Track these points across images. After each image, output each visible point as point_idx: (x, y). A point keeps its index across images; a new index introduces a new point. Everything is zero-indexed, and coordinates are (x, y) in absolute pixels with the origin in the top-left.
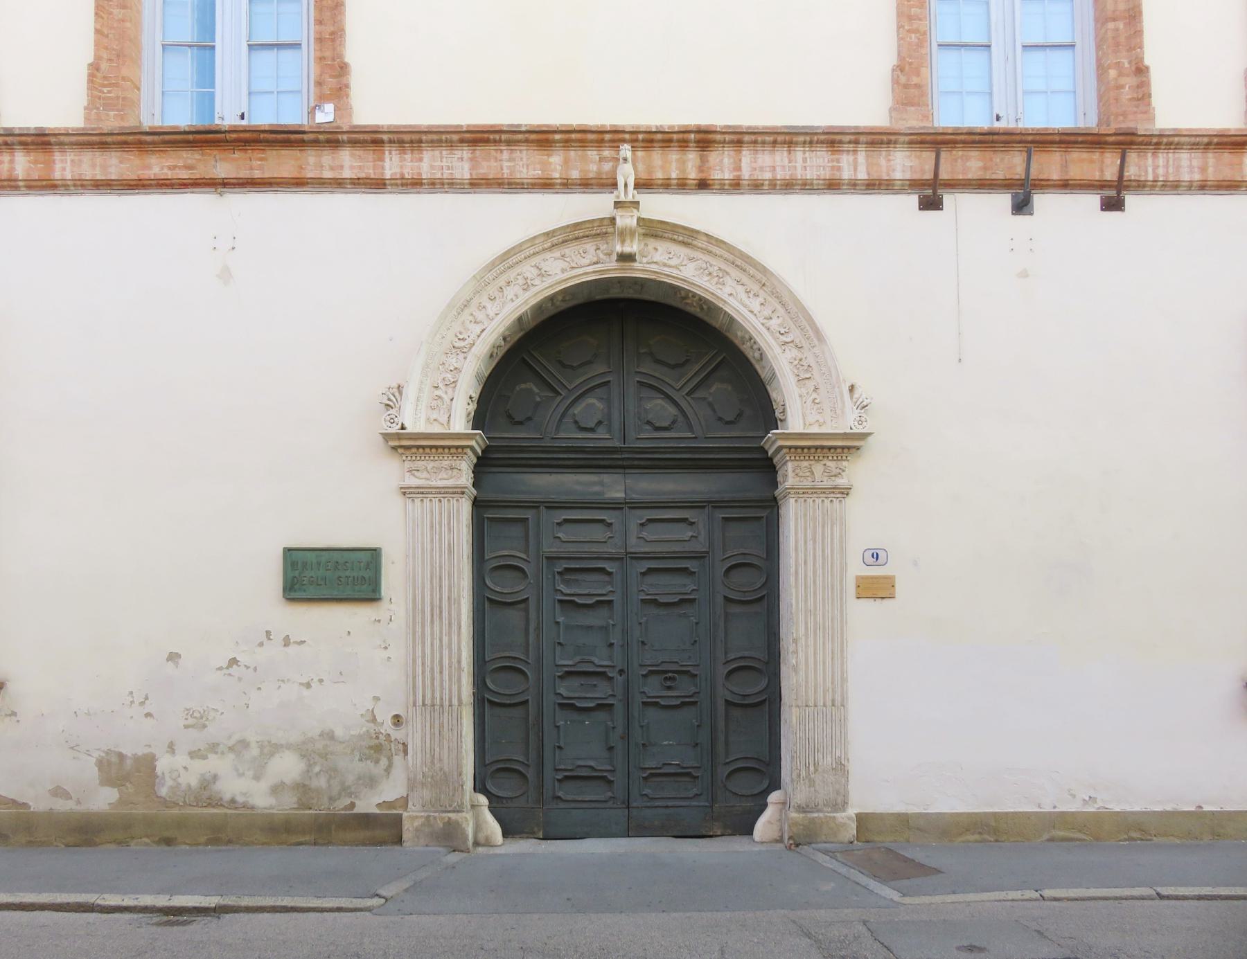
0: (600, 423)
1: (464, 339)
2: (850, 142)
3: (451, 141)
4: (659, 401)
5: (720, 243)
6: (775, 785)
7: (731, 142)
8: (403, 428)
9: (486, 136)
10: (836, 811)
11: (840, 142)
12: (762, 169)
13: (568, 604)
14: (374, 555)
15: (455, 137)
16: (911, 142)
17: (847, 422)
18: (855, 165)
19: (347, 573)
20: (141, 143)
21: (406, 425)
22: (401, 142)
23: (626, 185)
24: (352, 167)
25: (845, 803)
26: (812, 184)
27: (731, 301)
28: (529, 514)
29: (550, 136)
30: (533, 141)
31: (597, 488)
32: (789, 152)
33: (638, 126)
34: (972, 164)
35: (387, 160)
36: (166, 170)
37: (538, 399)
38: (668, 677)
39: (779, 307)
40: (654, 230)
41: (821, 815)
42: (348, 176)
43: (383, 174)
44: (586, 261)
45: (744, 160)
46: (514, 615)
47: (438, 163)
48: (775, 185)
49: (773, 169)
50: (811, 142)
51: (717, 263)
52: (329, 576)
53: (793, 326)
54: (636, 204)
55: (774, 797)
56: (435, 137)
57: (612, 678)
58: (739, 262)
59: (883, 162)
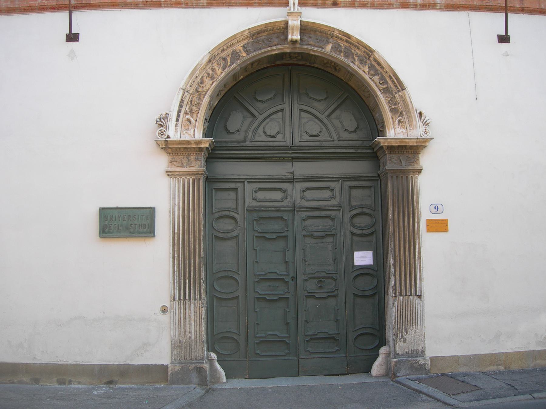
0: (278, 133)
6: (383, 342)
8: (168, 137)
13: (262, 238)
14: (152, 210)
19: (136, 222)
21: (170, 136)
23: (294, 4)
28: (239, 185)
38: (320, 281)
46: (231, 244)
48: (374, 4)
52: (123, 224)
54: (300, 14)
55: (383, 350)
57: (287, 282)
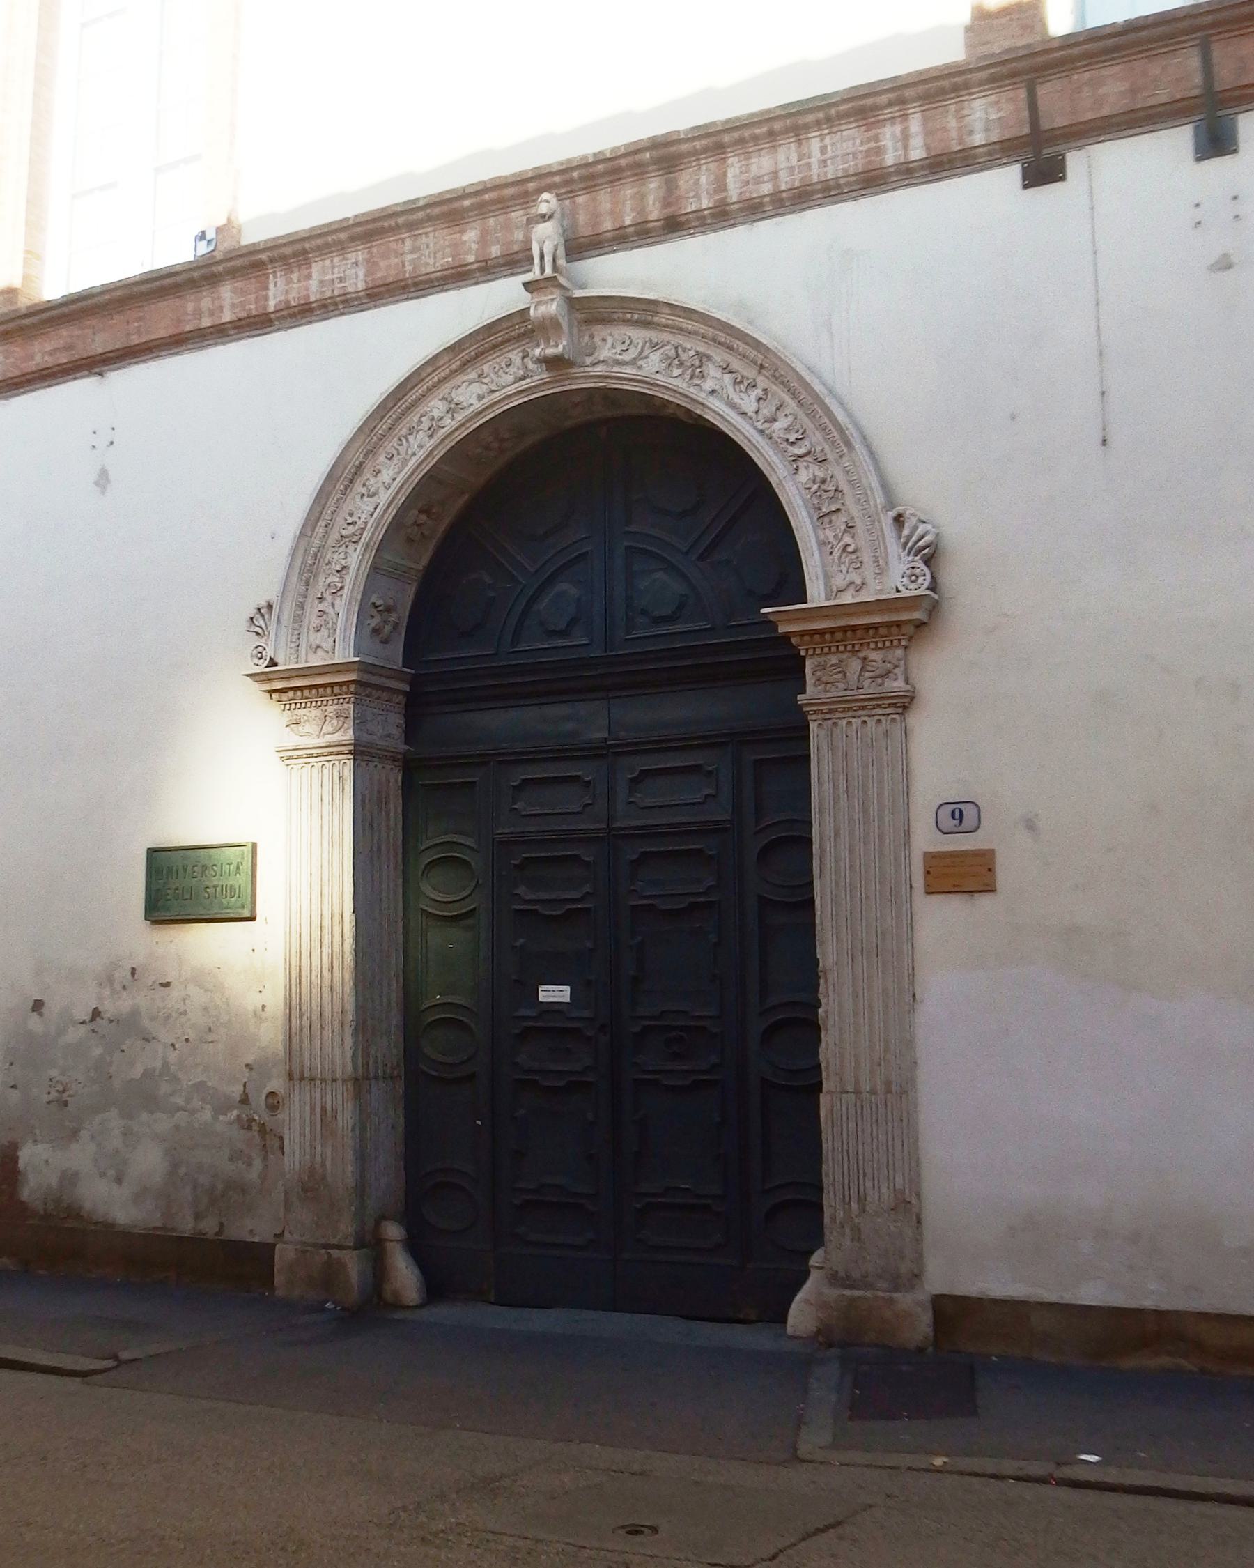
0: (573, 622)
1: (354, 523)
2: (891, 104)
3: (340, 242)
4: (659, 575)
5: (689, 313)
7: (705, 150)
8: (273, 663)
9: (378, 224)
10: (896, 1288)
11: (875, 108)
12: (758, 180)
15: (343, 236)
16: (993, 79)
17: (896, 576)
18: (906, 139)
20: (21, 328)
22: (284, 258)
24: (233, 306)
25: (917, 1276)
26: (838, 186)
27: (715, 403)
29: (457, 205)
30: (438, 217)
31: (569, 726)
32: (799, 142)
33: (570, 161)
34: (1111, 88)
35: (272, 286)
36: (46, 358)
37: (492, 594)
39: (787, 398)
40: (597, 313)
41: (869, 1294)
42: (227, 320)
43: (265, 307)
44: (511, 378)
45: (731, 173)
47: (329, 277)
49: (775, 175)
50: (828, 120)
51: (692, 346)
53: (810, 426)
56: (320, 241)
58: (722, 337)
59: (952, 123)
